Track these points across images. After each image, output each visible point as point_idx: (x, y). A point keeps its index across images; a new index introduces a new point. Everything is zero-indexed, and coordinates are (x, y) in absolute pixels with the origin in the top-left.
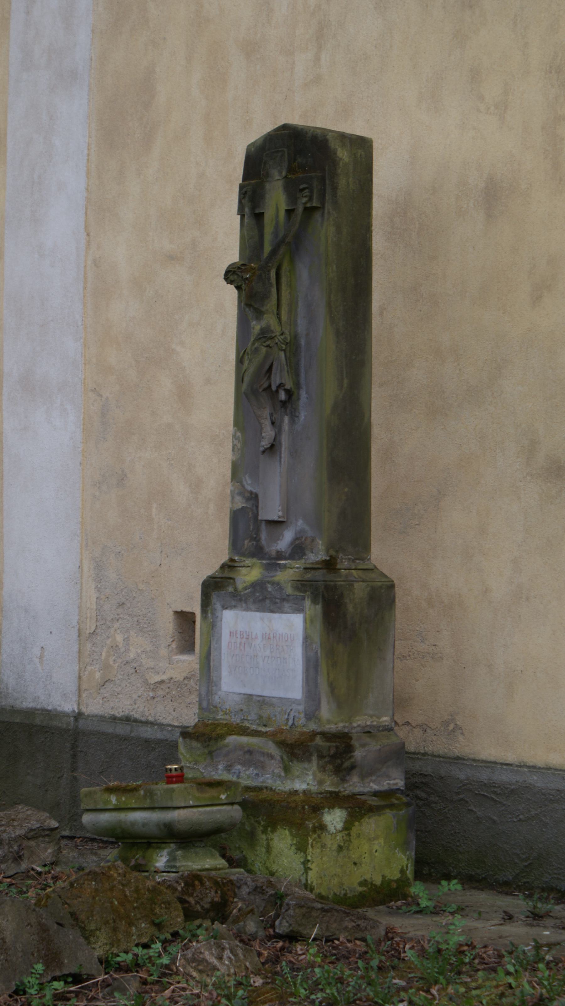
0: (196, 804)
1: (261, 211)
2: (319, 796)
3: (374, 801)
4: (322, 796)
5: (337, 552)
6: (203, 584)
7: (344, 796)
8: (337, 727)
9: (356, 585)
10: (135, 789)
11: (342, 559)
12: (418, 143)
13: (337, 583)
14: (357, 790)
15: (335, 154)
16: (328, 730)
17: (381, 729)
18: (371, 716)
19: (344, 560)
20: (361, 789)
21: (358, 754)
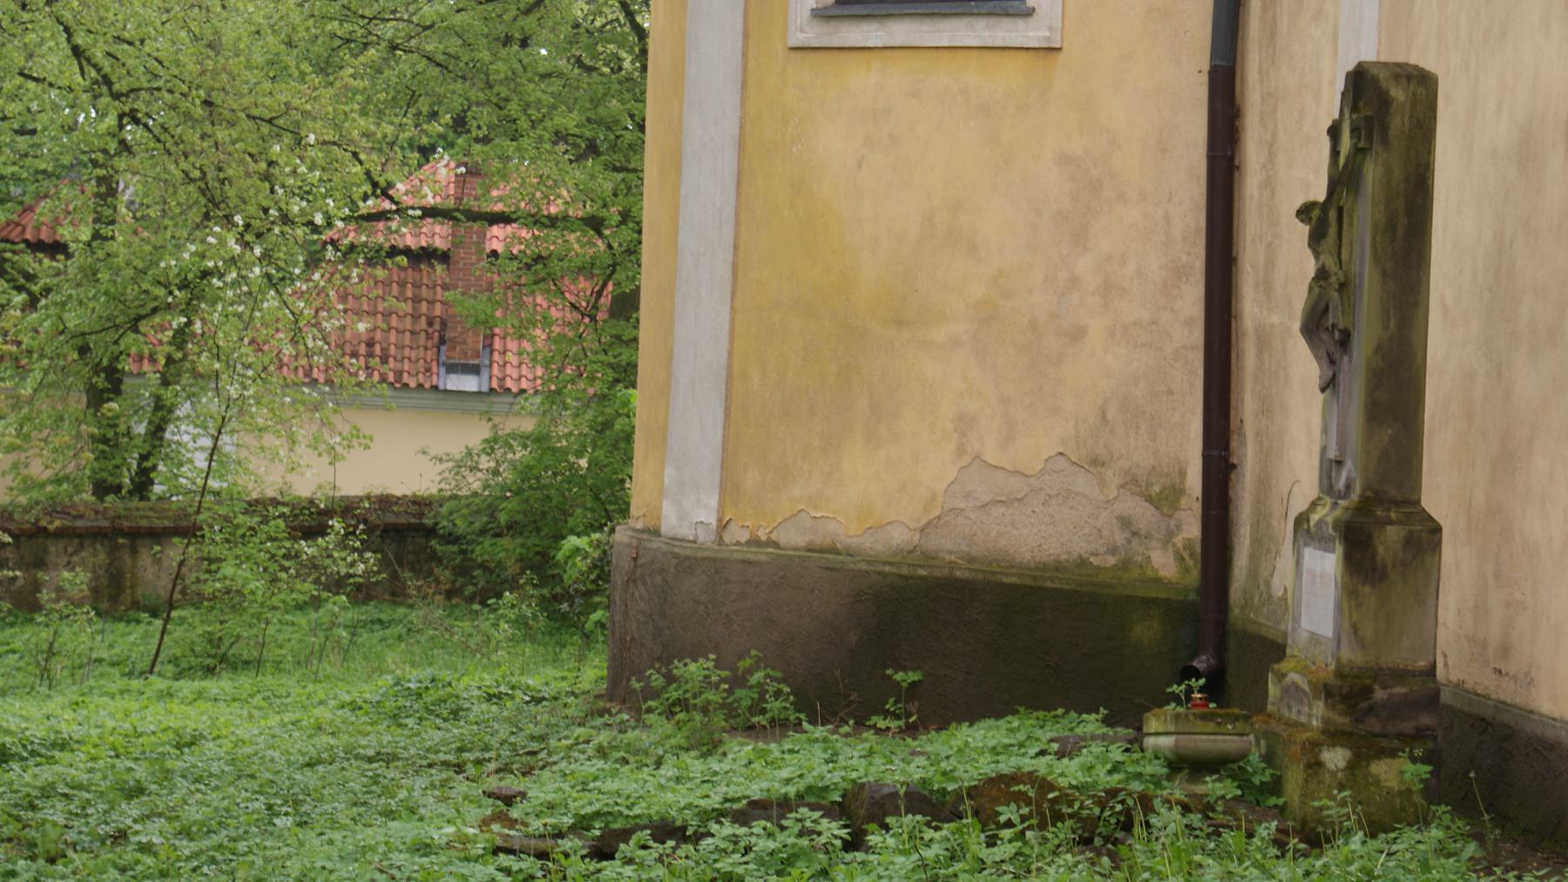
1: (1328, 104)
6: (1437, 529)
12: (1061, 56)
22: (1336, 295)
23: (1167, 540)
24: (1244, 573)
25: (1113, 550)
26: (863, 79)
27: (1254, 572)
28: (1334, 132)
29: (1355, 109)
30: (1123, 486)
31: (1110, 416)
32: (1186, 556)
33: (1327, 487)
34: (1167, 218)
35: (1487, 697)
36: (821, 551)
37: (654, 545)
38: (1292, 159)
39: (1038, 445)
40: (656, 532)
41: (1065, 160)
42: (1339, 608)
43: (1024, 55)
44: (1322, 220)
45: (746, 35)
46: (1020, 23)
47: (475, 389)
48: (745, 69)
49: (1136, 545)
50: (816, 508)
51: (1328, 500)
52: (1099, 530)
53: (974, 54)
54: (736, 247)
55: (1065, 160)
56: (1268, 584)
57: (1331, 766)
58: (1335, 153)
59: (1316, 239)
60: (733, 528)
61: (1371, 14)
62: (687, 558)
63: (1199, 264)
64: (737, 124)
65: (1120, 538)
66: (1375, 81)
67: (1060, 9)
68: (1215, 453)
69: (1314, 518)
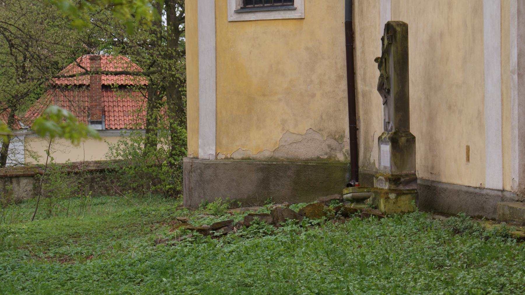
1: (380, 32)
3: (405, 192)
6: (414, 138)
10: (365, 198)
12: (305, 20)
23: (341, 150)
24: (362, 157)
25: (326, 154)
26: (250, 29)
27: (365, 157)
28: (383, 39)
29: (388, 33)
31: (323, 118)
33: (386, 129)
34: (336, 63)
35: (429, 180)
36: (246, 159)
37: (197, 161)
38: (371, 46)
39: (304, 126)
40: (197, 158)
41: (307, 49)
42: (391, 158)
43: (294, 21)
44: (381, 62)
45: (216, 18)
46: (293, 12)
47: (101, 129)
48: (216, 28)
49: (333, 152)
50: (243, 147)
51: (386, 132)
53: (281, 21)
54: (216, 77)
55: (307, 49)
56: (369, 159)
57: (391, 198)
58: (383, 44)
59: (380, 67)
60: (220, 154)
61: (389, 6)
62: (207, 164)
63: (345, 75)
64: (215, 43)
65: (328, 150)
66: (392, 26)
68: (352, 126)
69: (383, 137)
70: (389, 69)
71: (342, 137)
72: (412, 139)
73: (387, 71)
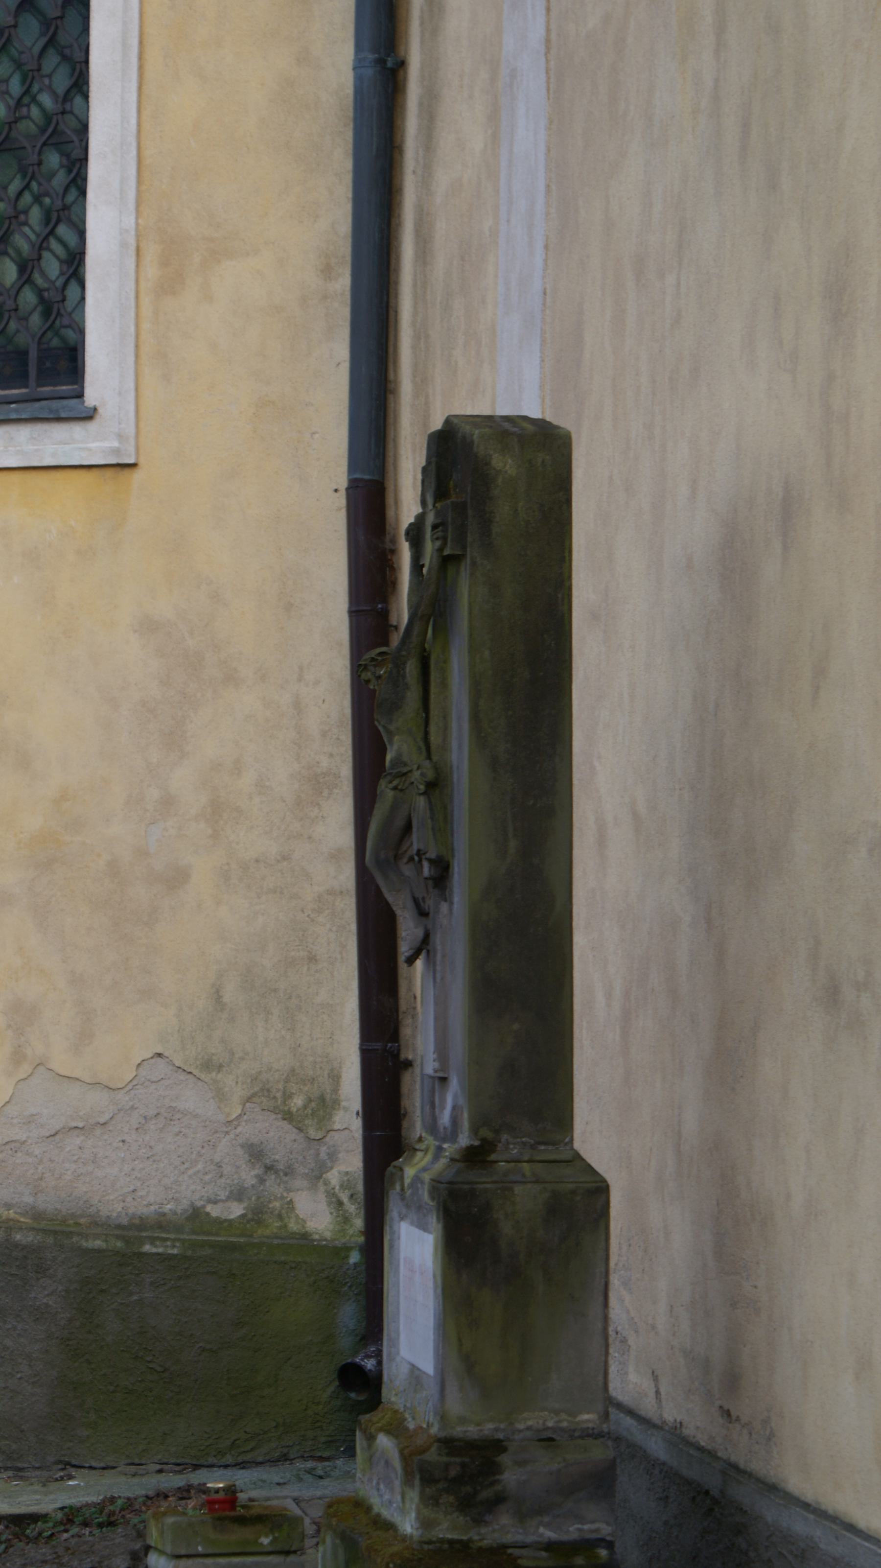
0: (210, 1551)
2: (426, 1547)
4: (431, 1547)
5: (497, 1132)
6: (600, 1190)
7: (480, 1548)
8: (481, 1430)
9: (518, 1189)
11: (508, 1143)
12: (137, 476)
13: (475, 1186)
14: (509, 1538)
15: (488, 464)
16: (461, 1435)
17: (577, 1434)
18: (557, 1412)
19: (512, 1146)
20: (519, 1538)
21: (511, 1477)
22: (421, 801)
23: (317, 1176)
25: (238, 1194)
30: (249, 1099)
31: (227, 998)
32: (344, 1197)
34: (298, 705)
35: (712, 1454)
39: (125, 1044)
41: (148, 627)
49: (272, 1185)
52: (219, 1165)
53: (15, 476)
55: (148, 627)
63: (346, 770)
65: (248, 1176)
66: (467, 444)
67: (132, 408)
70: (446, 728)
71: (324, 1106)
72: (582, 1206)
73: (434, 739)
